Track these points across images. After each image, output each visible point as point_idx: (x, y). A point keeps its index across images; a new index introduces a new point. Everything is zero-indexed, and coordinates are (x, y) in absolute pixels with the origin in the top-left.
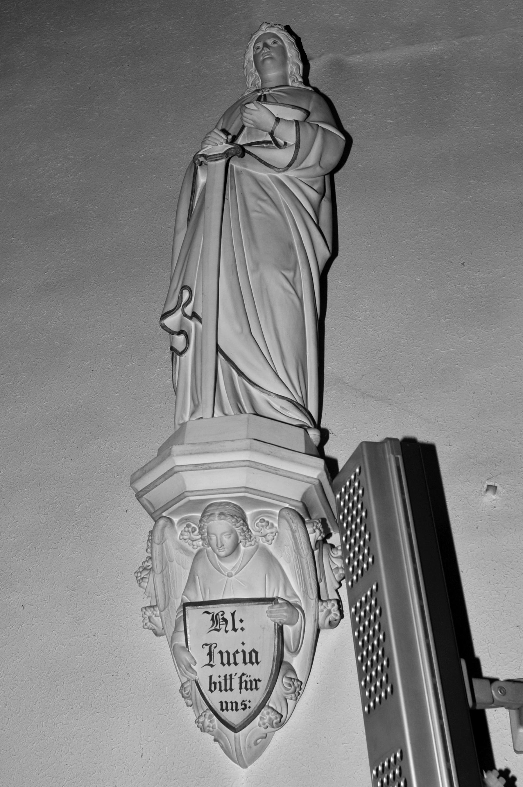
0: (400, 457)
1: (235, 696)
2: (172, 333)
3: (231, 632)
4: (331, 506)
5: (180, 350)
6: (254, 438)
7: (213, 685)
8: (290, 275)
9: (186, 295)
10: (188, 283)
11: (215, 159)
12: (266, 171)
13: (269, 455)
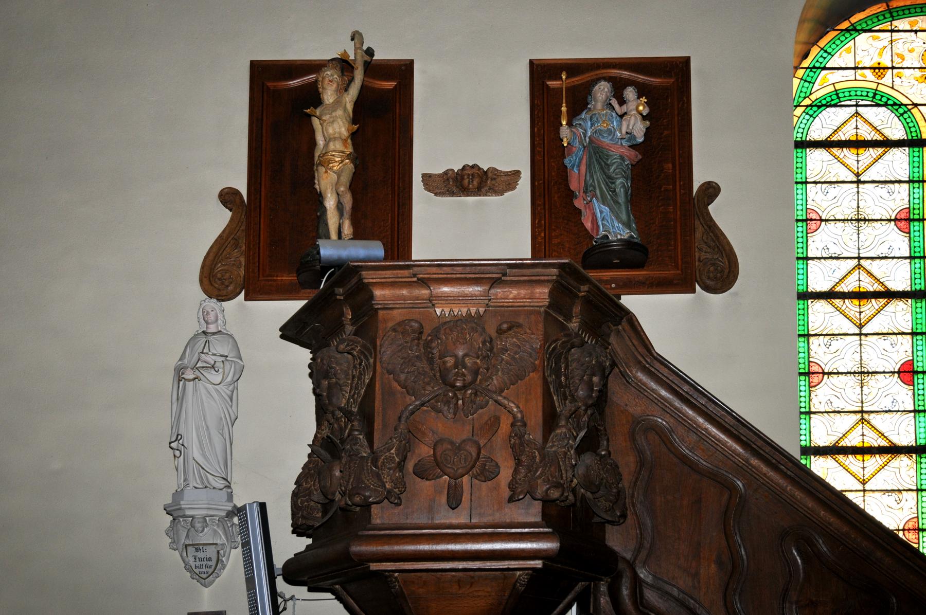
1: (204, 570)
3: (202, 553)
7: (196, 567)
8: (221, 431)
9: (179, 437)
10: (179, 433)
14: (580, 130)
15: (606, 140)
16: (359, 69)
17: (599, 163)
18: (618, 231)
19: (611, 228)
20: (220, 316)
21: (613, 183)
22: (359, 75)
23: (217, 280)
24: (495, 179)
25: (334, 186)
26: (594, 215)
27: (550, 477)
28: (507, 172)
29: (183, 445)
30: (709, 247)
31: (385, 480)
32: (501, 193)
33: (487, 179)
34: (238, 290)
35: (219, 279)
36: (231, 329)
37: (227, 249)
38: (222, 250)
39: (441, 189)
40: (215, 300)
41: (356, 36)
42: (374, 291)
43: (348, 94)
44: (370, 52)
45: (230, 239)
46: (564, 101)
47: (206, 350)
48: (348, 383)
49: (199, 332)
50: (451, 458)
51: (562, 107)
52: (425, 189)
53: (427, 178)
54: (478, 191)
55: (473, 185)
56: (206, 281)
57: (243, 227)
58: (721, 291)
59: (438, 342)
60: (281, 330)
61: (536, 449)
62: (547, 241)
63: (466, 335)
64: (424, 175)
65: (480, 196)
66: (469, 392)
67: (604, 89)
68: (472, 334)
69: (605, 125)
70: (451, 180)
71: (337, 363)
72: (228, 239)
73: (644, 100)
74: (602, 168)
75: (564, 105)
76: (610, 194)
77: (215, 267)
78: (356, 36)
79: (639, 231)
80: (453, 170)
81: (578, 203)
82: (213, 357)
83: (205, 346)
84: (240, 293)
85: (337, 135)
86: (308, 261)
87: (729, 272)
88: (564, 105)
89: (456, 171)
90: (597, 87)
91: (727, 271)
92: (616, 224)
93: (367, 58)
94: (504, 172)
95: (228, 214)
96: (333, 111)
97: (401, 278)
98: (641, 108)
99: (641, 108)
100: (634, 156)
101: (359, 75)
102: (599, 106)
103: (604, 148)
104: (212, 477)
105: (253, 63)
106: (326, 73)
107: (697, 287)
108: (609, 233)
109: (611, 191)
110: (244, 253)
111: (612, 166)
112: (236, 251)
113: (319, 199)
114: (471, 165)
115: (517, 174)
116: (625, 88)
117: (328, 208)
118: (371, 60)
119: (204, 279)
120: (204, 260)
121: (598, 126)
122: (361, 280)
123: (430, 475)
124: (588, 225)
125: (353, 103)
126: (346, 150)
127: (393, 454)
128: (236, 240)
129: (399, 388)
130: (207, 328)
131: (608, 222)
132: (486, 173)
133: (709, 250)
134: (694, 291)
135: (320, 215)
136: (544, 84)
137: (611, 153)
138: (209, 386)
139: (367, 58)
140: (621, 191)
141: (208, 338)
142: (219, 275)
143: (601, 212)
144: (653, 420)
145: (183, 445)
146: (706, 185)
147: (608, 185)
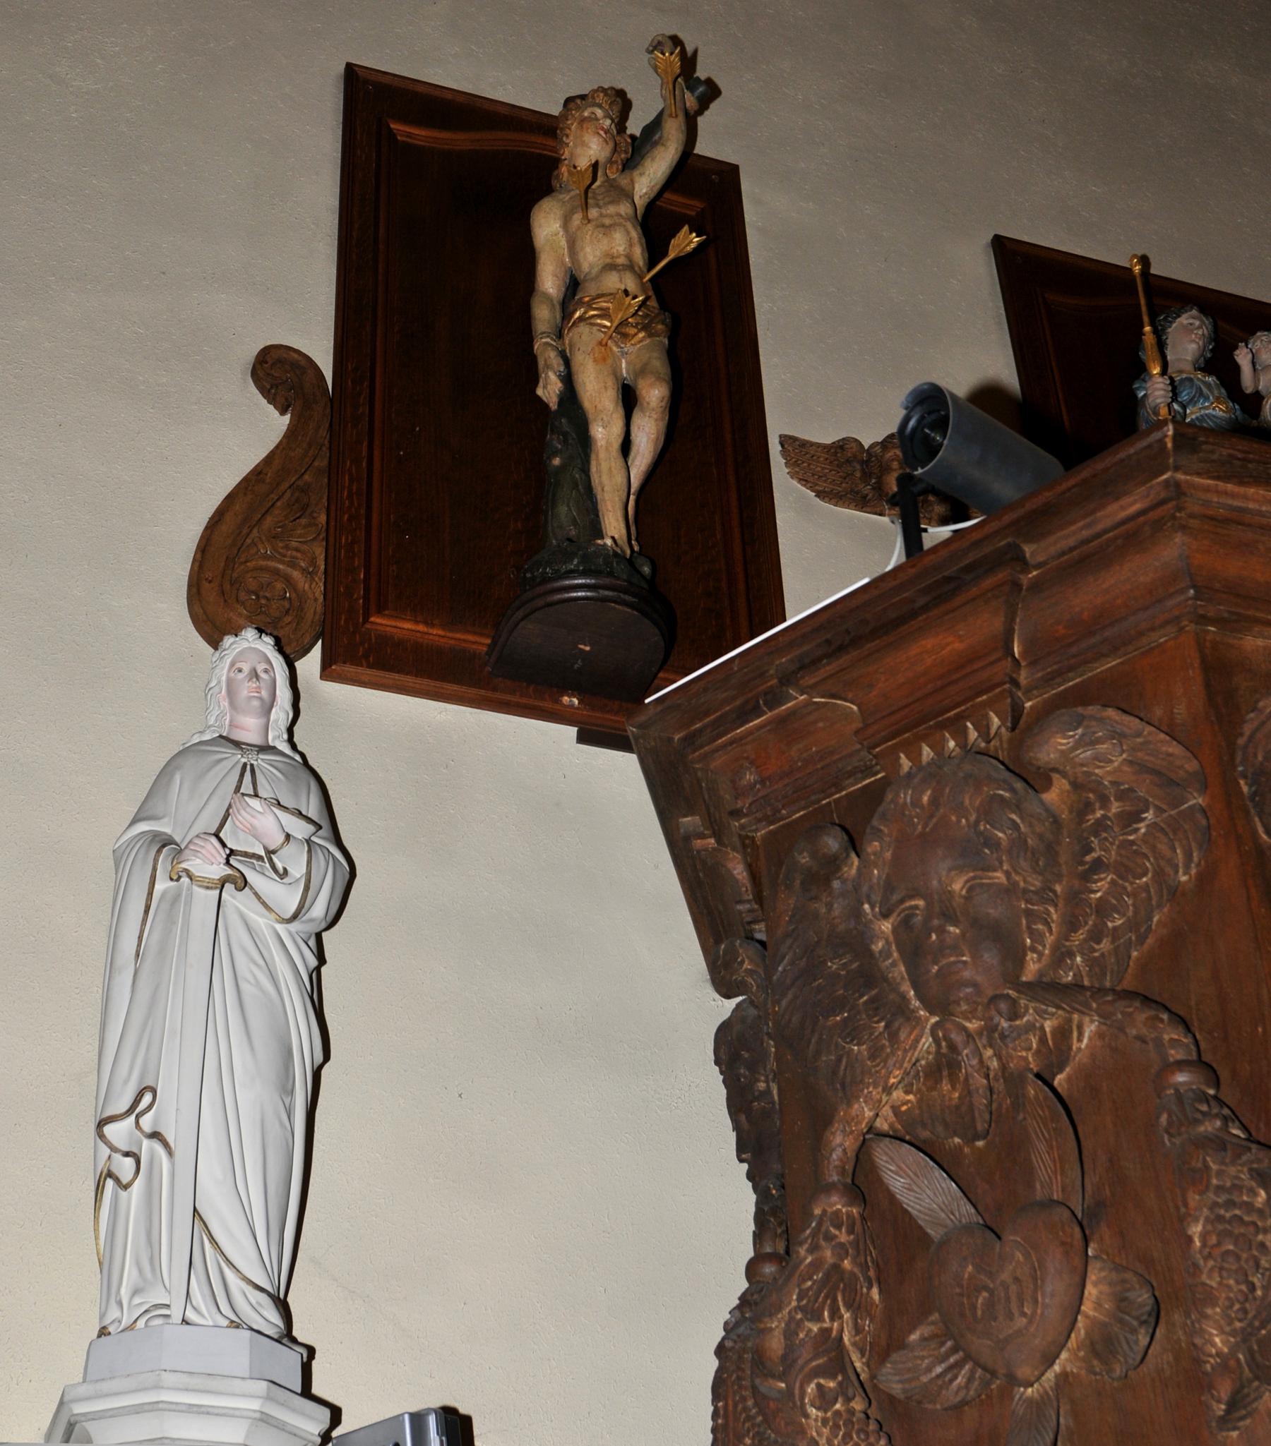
0: (444, 1438)
2: (114, 1149)
4: (84, 1364)
5: (125, 1181)
6: (270, 1379)
9: (147, 1098)
11: (205, 884)
12: (262, 916)
13: (283, 1404)
25: (558, 308)
34: (307, 640)
45: (285, 485)
47: (247, 787)
57: (322, 463)
64: (785, 440)
82: (286, 818)
85: (621, 261)
97: (136, 854)
104: (243, 1285)
110: (323, 535)
119: (205, 585)
120: (207, 528)
142: (252, 584)
144: (1053, 1039)
145: (155, 1135)
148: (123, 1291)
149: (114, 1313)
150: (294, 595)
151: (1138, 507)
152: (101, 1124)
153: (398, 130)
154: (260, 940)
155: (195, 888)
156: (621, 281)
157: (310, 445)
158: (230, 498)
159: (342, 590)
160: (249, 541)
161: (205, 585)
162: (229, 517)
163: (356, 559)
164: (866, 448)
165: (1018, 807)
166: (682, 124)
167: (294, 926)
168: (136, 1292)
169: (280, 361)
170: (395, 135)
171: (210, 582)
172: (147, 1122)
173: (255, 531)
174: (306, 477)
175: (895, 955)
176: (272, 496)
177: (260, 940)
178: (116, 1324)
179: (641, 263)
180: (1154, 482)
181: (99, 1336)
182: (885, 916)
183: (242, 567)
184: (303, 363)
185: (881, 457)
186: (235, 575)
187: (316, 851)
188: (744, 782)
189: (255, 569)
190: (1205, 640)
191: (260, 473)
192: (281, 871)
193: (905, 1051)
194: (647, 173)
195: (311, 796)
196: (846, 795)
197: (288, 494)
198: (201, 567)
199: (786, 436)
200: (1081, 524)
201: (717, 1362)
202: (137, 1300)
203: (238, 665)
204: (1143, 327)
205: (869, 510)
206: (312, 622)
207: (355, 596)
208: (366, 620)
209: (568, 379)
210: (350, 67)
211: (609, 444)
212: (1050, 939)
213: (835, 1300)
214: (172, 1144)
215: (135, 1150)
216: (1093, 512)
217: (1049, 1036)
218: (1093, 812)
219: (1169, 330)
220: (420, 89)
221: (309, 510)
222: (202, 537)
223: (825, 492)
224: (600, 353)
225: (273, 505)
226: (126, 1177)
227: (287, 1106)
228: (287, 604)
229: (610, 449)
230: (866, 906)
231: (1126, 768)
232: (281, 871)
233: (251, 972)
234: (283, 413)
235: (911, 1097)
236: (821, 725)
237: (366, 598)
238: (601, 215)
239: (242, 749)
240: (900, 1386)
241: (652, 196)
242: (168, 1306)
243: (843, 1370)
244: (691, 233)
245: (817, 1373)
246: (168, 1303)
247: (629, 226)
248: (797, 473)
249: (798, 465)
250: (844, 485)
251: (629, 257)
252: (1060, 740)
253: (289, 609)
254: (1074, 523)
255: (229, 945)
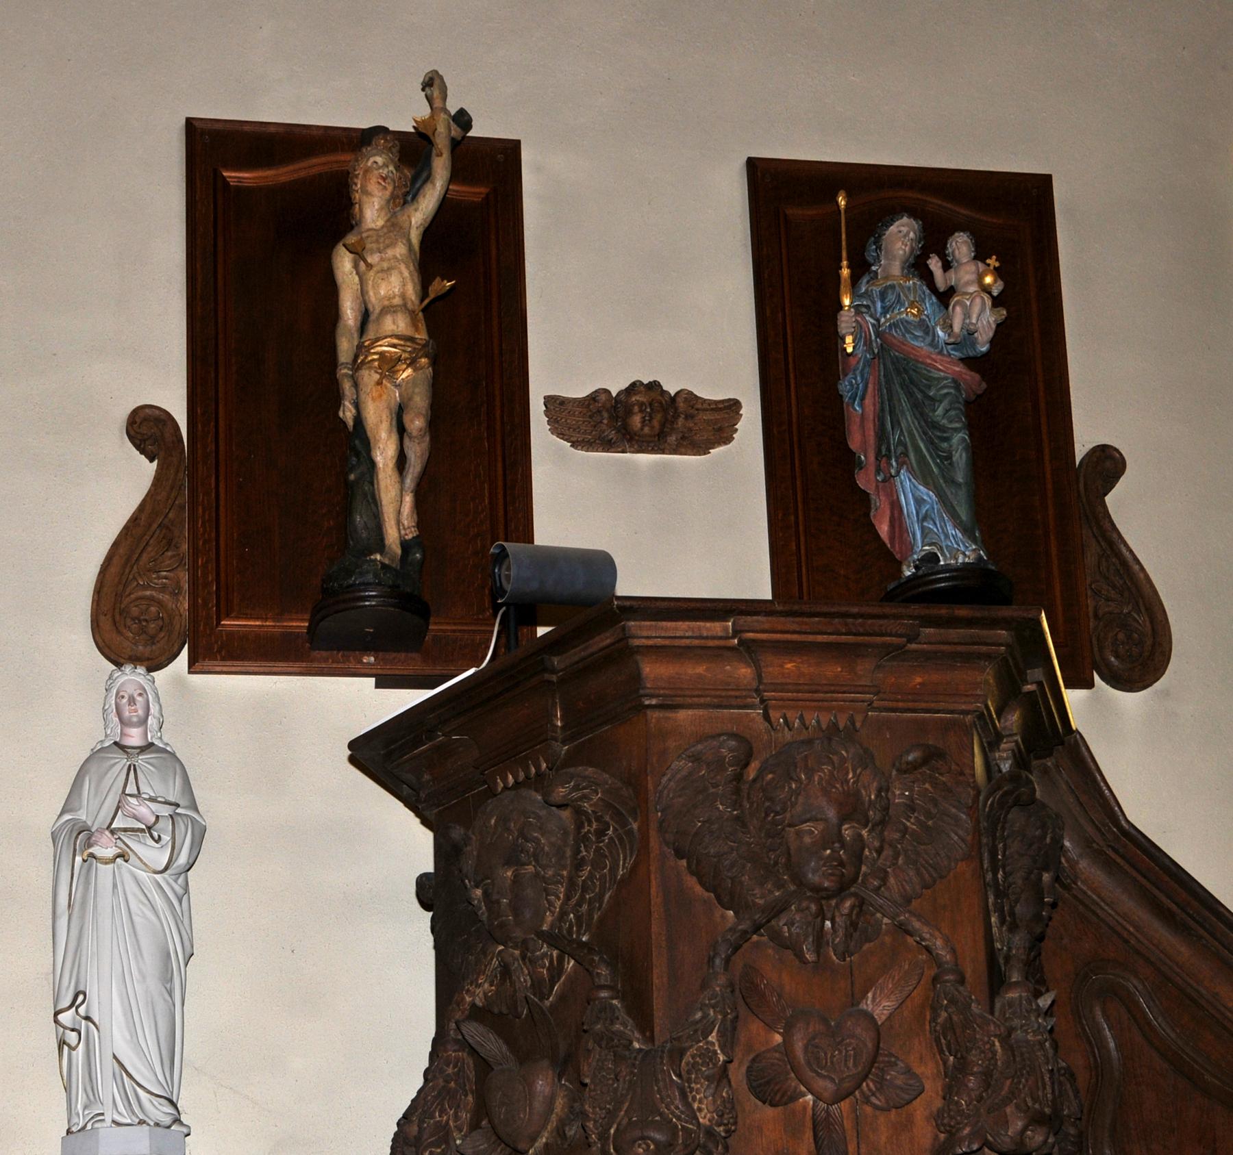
2: (65, 1028)
9: (81, 998)
14: (868, 318)
15: (919, 345)
16: (444, 155)
17: (910, 395)
18: (955, 546)
19: (942, 538)
20: (154, 709)
21: (947, 439)
22: (441, 168)
23: (129, 622)
24: (692, 417)
26: (896, 506)
27: (1029, 1100)
28: (716, 402)
29: (87, 1018)
30: (1114, 587)
31: (696, 1106)
32: (701, 448)
33: (676, 416)
35: (133, 619)
36: (170, 739)
37: (150, 549)
38: (139, 551)
39: (585, 432)
40: (141, 670)
41: (432, 84)
42: (642, 665)
43: (416, 210)
44: (463, 119)
45: (155, 526)
46: (844, 254)
47: (131, 789)
48: (562, 877)
49: (107, 744)
50: (826, 1054)
51: (841, 268)
52: (553, 431)
53: (553, 404)
54: (655, 443)
55: (652, 427)
56: (106, 623)
58: (1141, 685)
59: (790, 788)
60: (352, 745)
61: (995, 1036)
62: (803, 558)
63: (847, 773)
64: (550, 401)
65: (663, 453)
66: (848, 904)
67: (908, 233)
68: (858, 771)
69: (915, 311)
70: (605, 415)
71: (541, 829)
72: (150, 525)
73: (993, 262)
74: (916, 406)
75: (845, 263)
76: (936, 464)
77: (124, 590)
78: (432, 84)
79: (985, 544)
80: (607, 391)
81: (865, 480)
82: (153, 806)
83: (127, 779)
84: (176, 655)
85: (397, 301)
86: (351, 586)
87: (1153, 645)
88: (845, 263)
89: (614, 395)
90: (893, 229)
91: (1149, 642)
92: (951, 530)
93: (456, 132)
94: (710, 402)
95: (148, 469)
96: (388, 246)
98: (988, 280)
99: (988, 280)
100: (971, 379)
101: (441, 168)
102: (896, 269)
103: (922, 363)
104: (148, 1096)
105: (193, 128)
106: (372, 160)
107: (1096, 677)
108: (941, 549)
109: (939, 456)
111: (941, 402)
112: (170, 554)
113: (358, 439)
114: (645, 382)
115: (732, 408)
116: (953, 234)
117: (381, 465)
118: (464, 137)
119: (102, 618)
120: (100, 573)
121: (900, 313)
122: (625, 637)
123: (776, 1094)
124: (884, 529)
125: (422, 229)
126: (417, 336)
127: (713, 1044)
128: (167, 528)
129: (699, 889)
130: (123, 734)
131: (935, 524)
132: (673, 399)
133: (1113, 594)
134: (1089, 685)
135: (357, 481)
136: (217, 175)
137: (936, 374)
138: (142, 875)
139: (456, 132)
140: (960, 457)
141: (133, 761)
142: (135, 611)
143: (919, 502)
145: (87, 1018)
146: (1098, 454)
147: (932, 443)
148: (79, 1106)
149: (75, 1120)
150: (165, 615)
151: (608, 641)
152: (56, 1014)
153: (230, 177)
154: (146, 888)
155: (99, 865)
156: (394, 323)
157: (172, 488)
158: (116, 545)
159: (200, 601)
160: (131, 577)
161: (102, 618)
162: (116, 560)
163: (210, 575)
164: (614, 395)
165: (540, 828)
166: (447, 162)
167: (165, 875)
168: (85, 1108)
169: (146, 419)
170: (228, 183)
171: (105, 615)
172: (82, 1010)
173: (135, 567)
174: (170, 515)
175: (484, 908)
176: (146, 537)
177: (146, 888)
178: (76, 1126)
179: (413, 298)
180: (617, 626)
181: (67, 1134)
182: (477, 887)
183: (128, 599)
184: (163, 417)
185: (627, 401)
186: (123, 606)
187: (178, 823)
188: (424, 780)
189: (137, 599)
190: (652, 718)
191: (136, 519)
192: (157, 837)
193: (486, 966)
194: (420, 208)
195: (177, 777)
196: (478, 792)
197: (158, 532)
198: (98, 605)
199: (549, 397)
200: (581, 647)
201: (396, 1129)
202: (86, 1112)
203: (121, 694)
204: (841, 261)
205: (613, 450)
206: (179, 633)
207: (210, 605)
208: (218, 624)
209: (357, 405)
210: (190, 123)
211: (385, 465)
212: (558, 904)
213: (443, 1105)
214: (97, 1023)
215: (77, 1027)
216: (587, 641)
217: (555, 959)
218: (584, 828)
219: (884, 237)
220: (246, 128)
221: (173, 543)
222: (97, 581)
223: (578, 441)
224: (377, 391)
225: (147, 544)
226: (74, 1043)
227: (169, 989)
228: (160, 623)
229: (387, 470)
230: (467, 881)
231: (600, 803)
232: (157, 837)
233: (141, 909)
234: (151, 461)
235: (493, 988)
236: (461, 749)
237: (218, 605)
238: (382, 260)
239: (127, 753)
240: (471, 1150)
241: (426, 225)
242: (102, 1114)
243: (447, 1143)
244: (442, 281)
245: (432, 1145)
246: (102, 1112)
247: (403, 267)
248: (557, 428)
249: (558, 422)
250: (594, 433)
251: (403, 296)
252: (561, 790)
253: (162, 627)
254: (576, 647)
255: (125, 894)
